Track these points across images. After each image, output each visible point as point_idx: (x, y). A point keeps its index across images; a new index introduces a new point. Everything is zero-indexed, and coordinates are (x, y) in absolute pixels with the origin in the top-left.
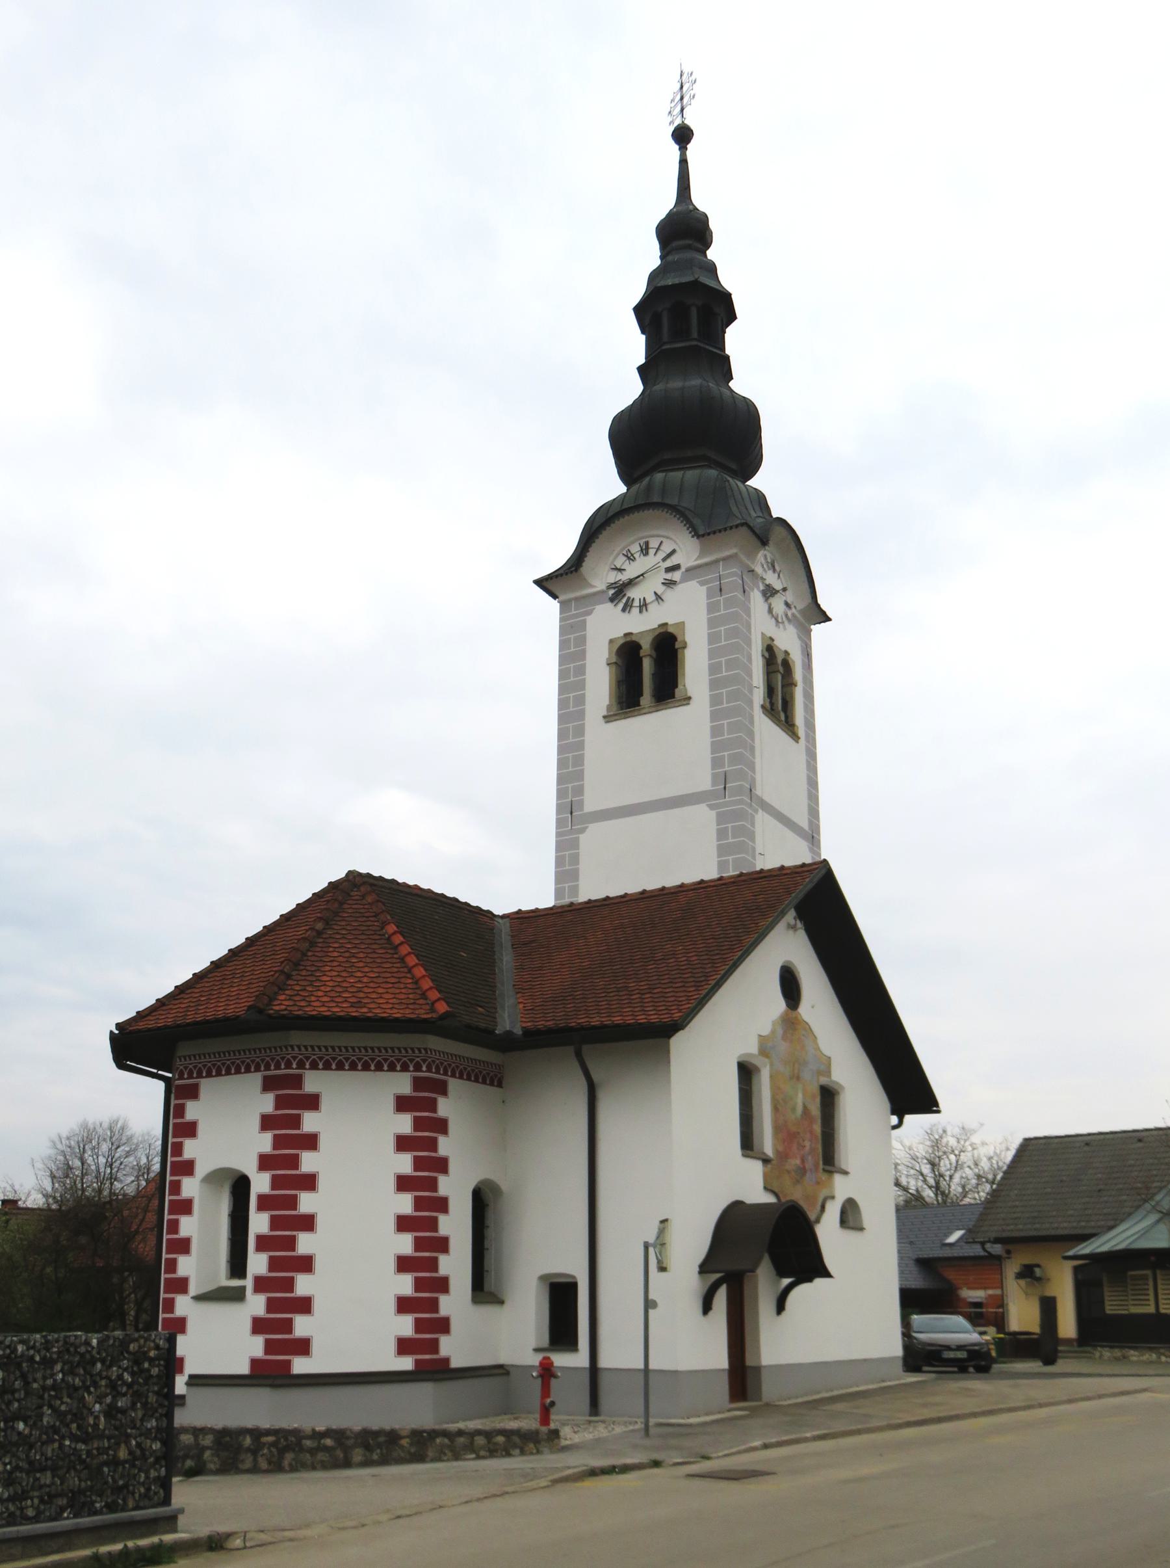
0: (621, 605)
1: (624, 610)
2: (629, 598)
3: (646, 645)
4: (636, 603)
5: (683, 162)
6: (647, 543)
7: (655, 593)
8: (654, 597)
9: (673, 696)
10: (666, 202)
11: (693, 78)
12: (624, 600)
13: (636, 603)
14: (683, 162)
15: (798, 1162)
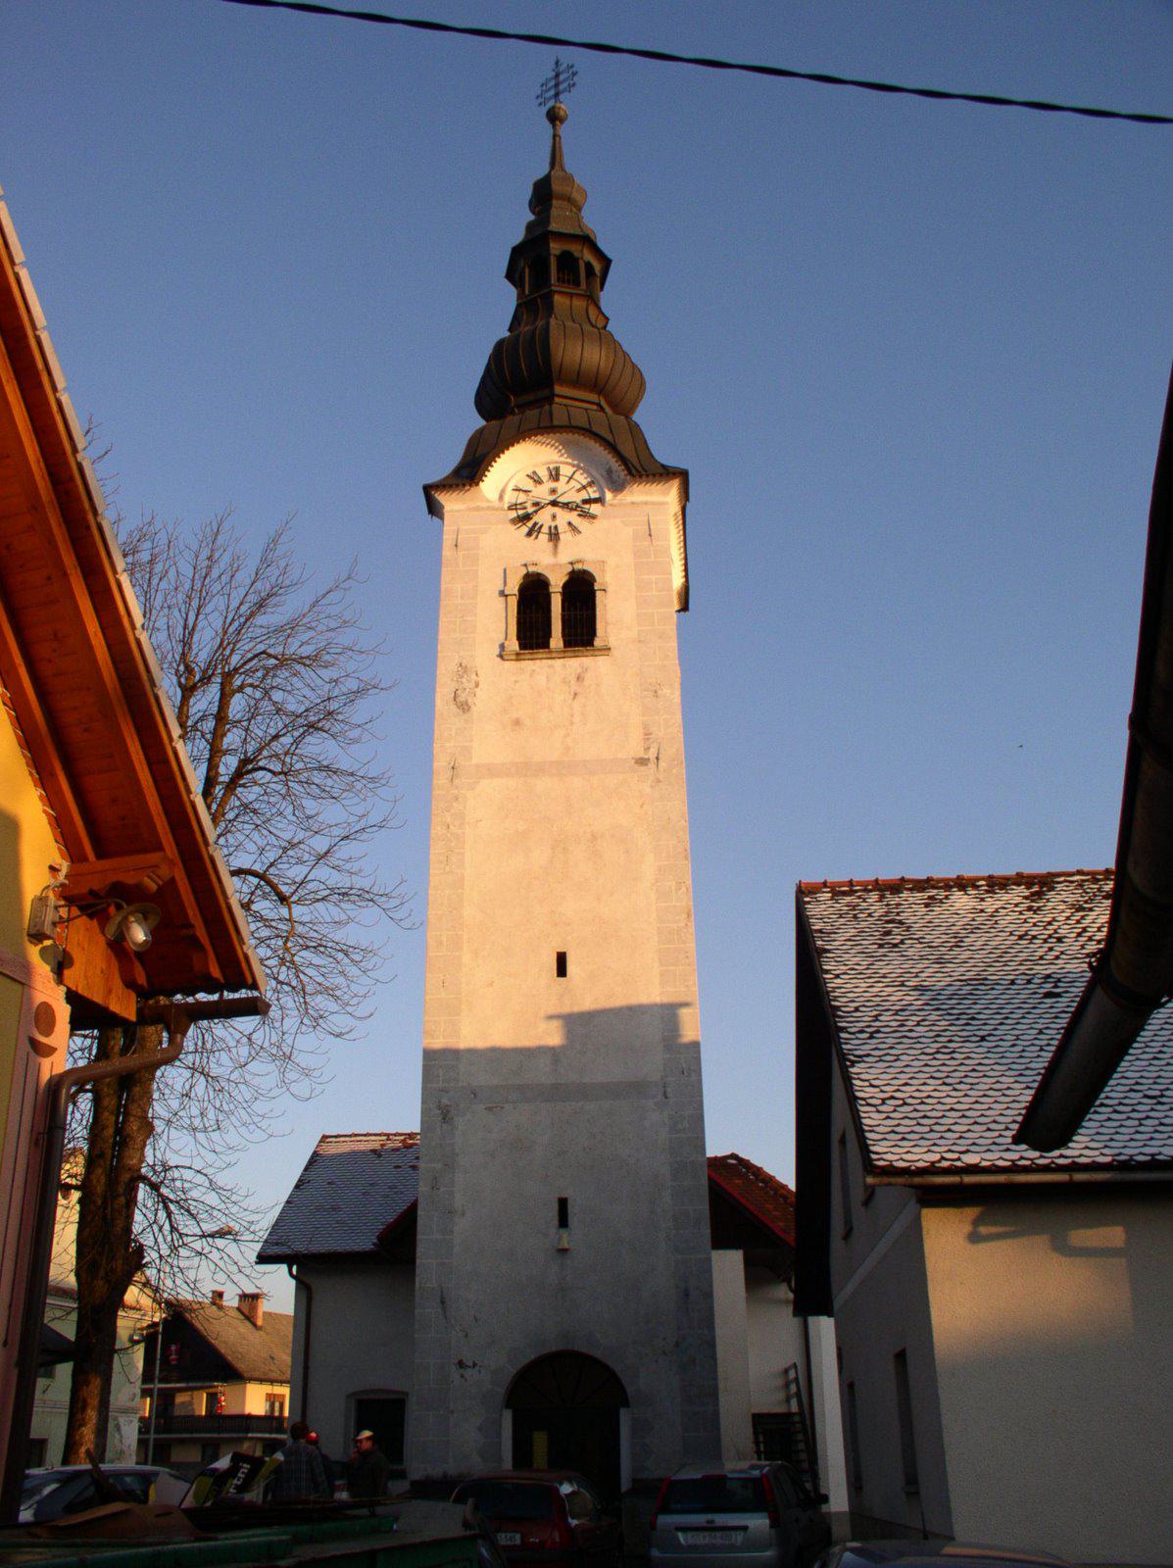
0: (525, 530)
1: (529, 534)
2: (535, 524)
3: (557, 581)
4: (545, 529)
6: (557, 469)
7: (570, 524)
8: (567, 528)
9: (591, 644)
10: (542, 170)
11: (574, 69)
12: (530, 524)
13: (545, 529)
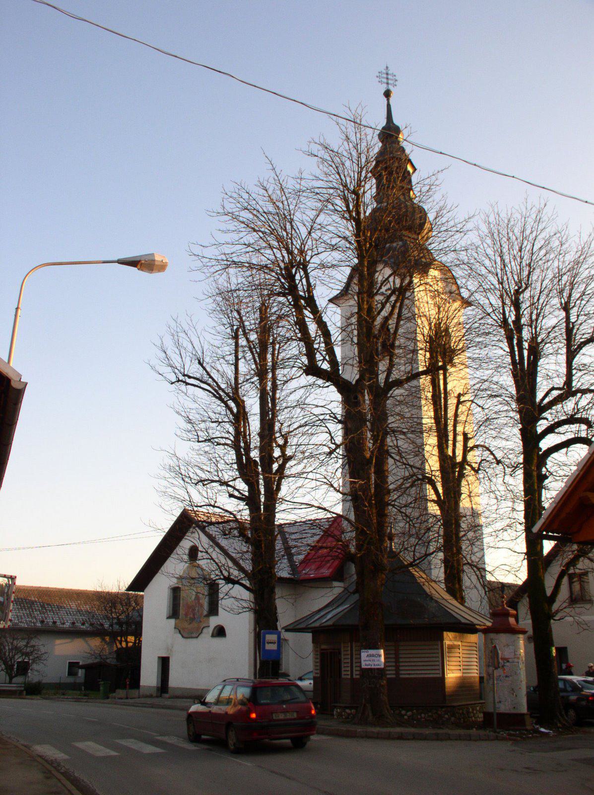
5: (389, 106)
14: (389, 106)
15: (192, 616)
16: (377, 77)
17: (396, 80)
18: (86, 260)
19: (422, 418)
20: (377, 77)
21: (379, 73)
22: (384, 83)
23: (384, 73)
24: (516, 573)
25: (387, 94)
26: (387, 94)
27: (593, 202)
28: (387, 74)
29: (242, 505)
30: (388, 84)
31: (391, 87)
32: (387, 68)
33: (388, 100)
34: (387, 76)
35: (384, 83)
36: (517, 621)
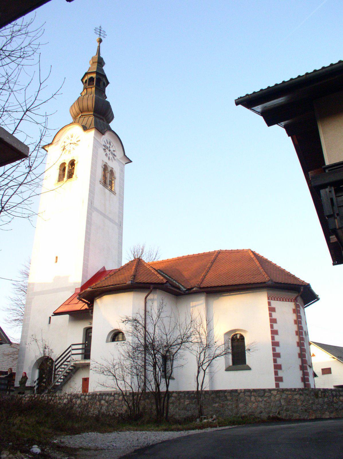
5: (99, 47)
14: (99, 47)
16: (106, 35)
17: (95, 30)
18: (78, 345)
19: (14, 403)
20: (106, 35)
21: (96, 28)
22: (98, 34)
23: (98, 29)
24: (119, 323)
25: (100, 41)
26: (100, 41)
27: (1, 67)
28: (100, 30)
29: (152, 341)
30: (100, 35)
31: (102, 37)
32: (100, 27)
33: (100, 44)
34: (100, 31)
35: (98, 34)
36: (135, 322)
